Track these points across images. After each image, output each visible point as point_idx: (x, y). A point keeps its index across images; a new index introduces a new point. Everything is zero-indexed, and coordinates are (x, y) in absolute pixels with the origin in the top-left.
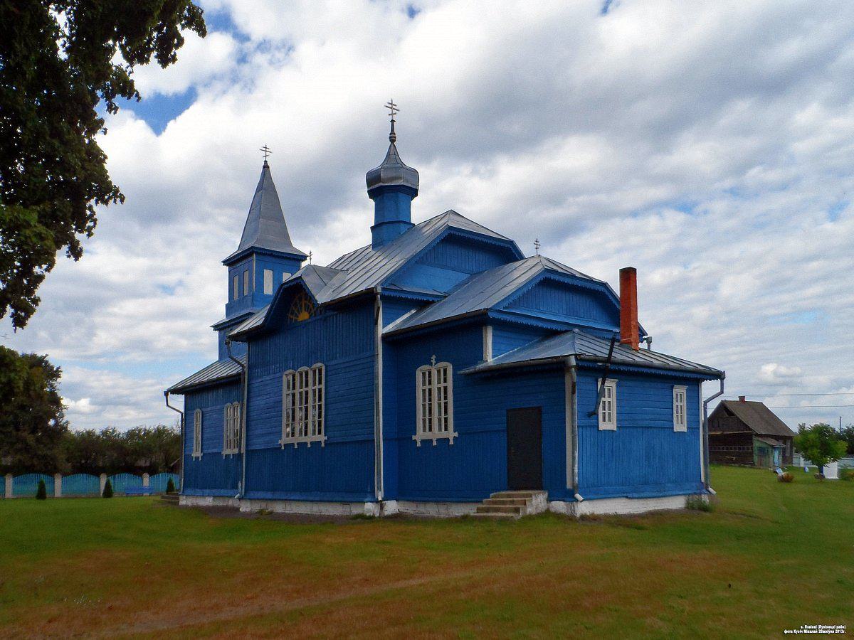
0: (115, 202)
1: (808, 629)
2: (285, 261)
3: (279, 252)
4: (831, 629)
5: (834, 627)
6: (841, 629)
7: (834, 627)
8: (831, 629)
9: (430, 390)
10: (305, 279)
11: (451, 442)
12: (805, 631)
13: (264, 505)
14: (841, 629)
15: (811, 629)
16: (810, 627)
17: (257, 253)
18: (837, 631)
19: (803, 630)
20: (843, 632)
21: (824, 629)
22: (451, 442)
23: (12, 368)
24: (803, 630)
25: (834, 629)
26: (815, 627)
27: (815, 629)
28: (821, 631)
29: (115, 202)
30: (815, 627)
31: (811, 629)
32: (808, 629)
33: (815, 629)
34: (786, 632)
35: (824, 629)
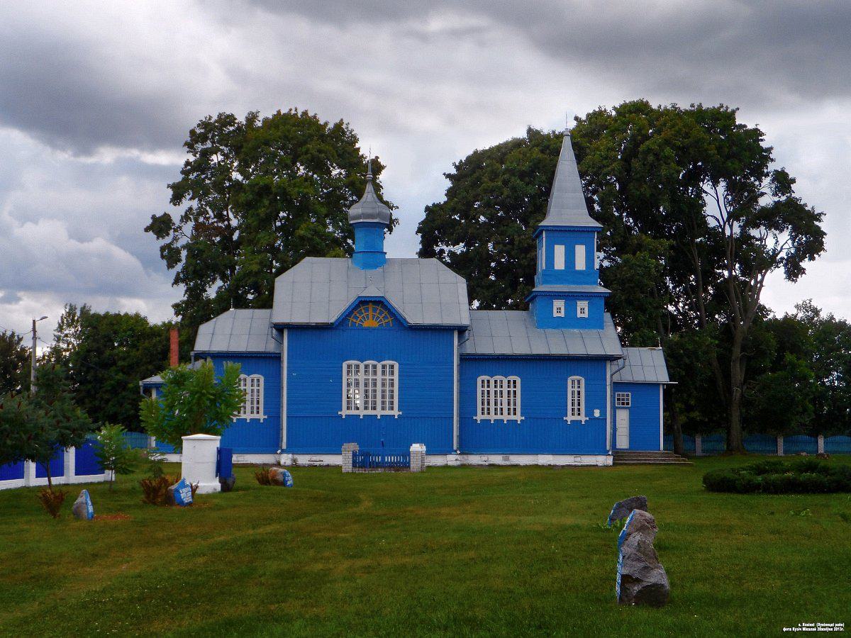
0: (762, 140)
1: (806, 627)
2: (568, 234)
3: (574, 227)
4: (829, 627)
5: (832, 625)
6: (839, 626)
7: (832, 625)
8: (829, 627)
9: (488, 392)
10: (268, 311)
11: (583, 423)
12: (804, 629)
13: (696, 257)
14: (839, 626)
15: (810, 627)
16: (823, 625)
17: (547, 231)
18: (836, 629)
19: (801, 627)
20: (842, 629)
21: (823, 627)
22: (583, 423)
23: (61, 438)
24: (801, 627)
25: (833, 627)
26: (813, 625)
27: (812, 627)
28: (820, 629)
29: (762, 140)
30: (813, 625)
31: (810, 627)
32: (806, 627)
33: (812, 627)
34: (785, 629)
35: (823, 627)
